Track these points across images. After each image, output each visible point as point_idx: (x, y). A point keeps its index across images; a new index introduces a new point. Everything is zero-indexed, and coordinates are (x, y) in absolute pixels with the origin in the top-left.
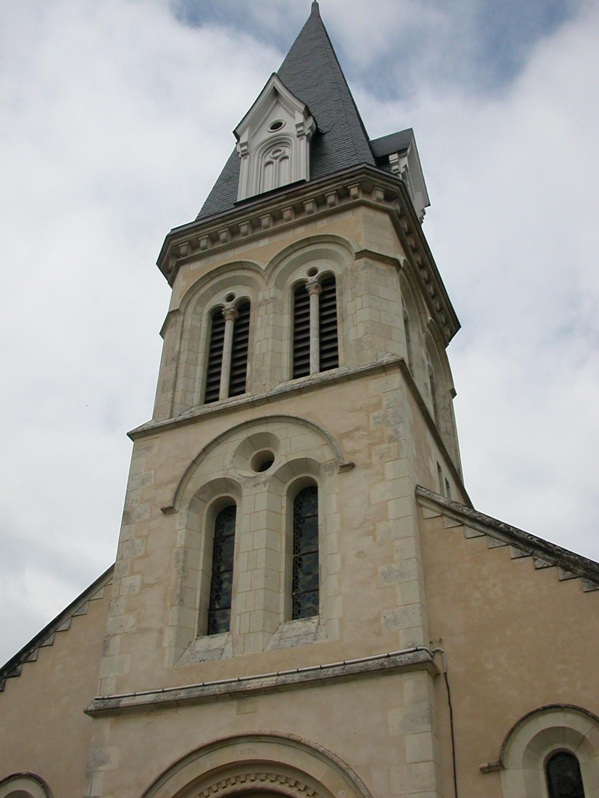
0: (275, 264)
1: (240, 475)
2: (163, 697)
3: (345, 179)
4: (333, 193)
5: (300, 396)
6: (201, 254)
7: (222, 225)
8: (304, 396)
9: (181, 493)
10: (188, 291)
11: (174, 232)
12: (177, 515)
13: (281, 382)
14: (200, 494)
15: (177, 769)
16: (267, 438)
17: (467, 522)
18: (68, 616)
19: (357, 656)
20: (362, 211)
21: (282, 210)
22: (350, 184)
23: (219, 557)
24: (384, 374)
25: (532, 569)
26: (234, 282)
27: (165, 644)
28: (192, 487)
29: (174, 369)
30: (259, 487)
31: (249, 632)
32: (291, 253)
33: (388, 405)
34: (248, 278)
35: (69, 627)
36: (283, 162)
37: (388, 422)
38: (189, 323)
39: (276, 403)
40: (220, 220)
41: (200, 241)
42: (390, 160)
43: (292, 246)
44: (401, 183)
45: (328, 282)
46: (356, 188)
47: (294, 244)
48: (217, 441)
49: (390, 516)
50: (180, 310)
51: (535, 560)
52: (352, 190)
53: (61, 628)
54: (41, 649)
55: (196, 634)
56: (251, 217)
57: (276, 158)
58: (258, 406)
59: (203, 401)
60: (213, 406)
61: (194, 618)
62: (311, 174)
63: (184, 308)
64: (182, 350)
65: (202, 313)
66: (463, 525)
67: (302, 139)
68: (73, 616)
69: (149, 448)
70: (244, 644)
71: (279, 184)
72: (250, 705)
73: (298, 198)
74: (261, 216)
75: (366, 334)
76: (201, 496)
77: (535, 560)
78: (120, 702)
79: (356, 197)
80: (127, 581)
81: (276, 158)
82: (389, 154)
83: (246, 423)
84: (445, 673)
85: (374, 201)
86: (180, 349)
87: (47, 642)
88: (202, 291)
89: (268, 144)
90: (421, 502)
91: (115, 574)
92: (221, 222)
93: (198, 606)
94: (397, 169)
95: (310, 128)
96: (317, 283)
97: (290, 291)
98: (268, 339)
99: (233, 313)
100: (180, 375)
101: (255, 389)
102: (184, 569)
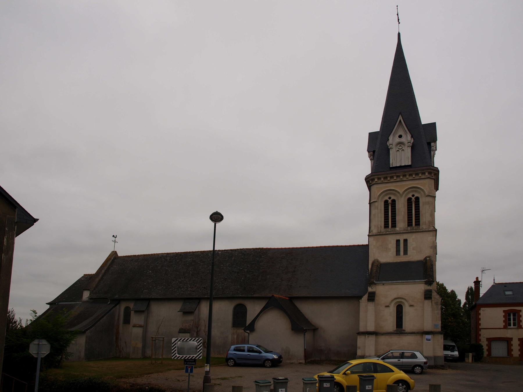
36: (403, 151)
45: (417, 199)
67: (409, 148)
94: (433, 149)
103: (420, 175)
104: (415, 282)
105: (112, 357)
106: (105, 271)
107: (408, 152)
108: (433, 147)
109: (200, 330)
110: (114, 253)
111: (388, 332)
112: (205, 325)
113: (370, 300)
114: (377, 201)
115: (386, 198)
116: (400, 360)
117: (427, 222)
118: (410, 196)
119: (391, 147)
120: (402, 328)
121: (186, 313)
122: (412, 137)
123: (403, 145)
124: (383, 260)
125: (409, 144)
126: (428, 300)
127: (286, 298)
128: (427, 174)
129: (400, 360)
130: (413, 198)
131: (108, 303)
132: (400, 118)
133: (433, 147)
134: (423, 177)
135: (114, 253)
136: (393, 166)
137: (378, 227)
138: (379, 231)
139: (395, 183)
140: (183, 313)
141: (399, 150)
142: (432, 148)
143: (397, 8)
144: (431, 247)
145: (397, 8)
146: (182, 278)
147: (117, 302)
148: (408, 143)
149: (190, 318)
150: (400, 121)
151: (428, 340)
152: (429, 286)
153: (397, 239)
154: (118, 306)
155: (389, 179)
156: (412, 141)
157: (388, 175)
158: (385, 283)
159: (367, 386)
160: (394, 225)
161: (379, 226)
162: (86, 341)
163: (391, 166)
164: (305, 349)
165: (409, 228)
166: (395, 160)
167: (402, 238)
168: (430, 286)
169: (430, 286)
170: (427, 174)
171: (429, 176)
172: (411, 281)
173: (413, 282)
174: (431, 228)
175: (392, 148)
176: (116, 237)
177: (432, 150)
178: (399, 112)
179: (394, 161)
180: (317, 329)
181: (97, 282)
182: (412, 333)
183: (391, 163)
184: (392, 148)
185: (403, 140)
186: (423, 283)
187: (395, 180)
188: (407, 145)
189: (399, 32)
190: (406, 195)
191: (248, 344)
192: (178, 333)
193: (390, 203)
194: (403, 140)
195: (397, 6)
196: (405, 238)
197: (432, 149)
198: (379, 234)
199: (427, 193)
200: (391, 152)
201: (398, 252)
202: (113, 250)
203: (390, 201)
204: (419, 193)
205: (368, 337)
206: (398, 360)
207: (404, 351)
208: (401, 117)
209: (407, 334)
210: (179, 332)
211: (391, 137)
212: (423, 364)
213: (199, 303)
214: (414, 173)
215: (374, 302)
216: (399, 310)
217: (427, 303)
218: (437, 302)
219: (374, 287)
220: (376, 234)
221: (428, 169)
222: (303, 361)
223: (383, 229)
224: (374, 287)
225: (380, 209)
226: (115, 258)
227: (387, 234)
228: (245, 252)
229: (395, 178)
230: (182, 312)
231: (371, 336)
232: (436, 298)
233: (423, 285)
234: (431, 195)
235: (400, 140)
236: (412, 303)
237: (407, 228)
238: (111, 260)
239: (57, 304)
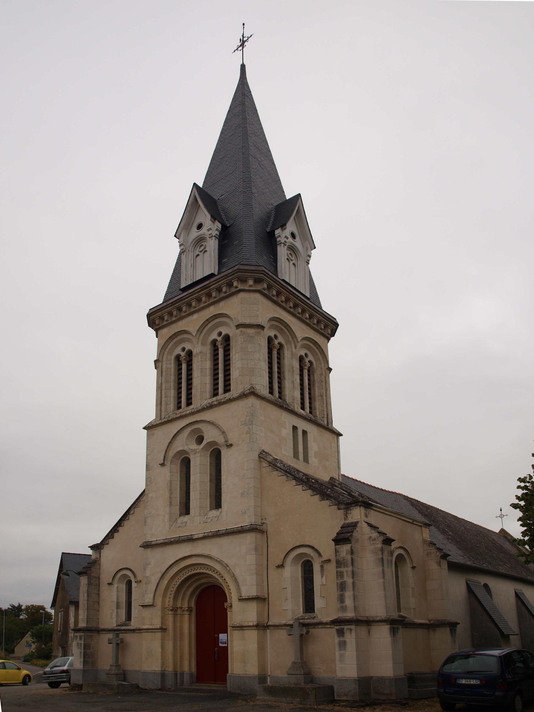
0: (200, 331)
1: (189, 448)
2: (166, 541)
3: (229, 276)
4: (224, 285)
6: (166, 324)
7: (172, 307)
8: (214, 409)
9: (166, 457)
10: (162, 348)
11: (151, 312)
12: (166, 467)
13: (206, 400)
14: (175, 457)
15: (172, 567)
16: (199, 430)
17: (278, 469)
18: (133, 508)
19: (231, 526)
20: (242, 295)
21: (201, 297)
23: (248, 418)
24: (246, 399)
25: (301, 490)
27: (166, 520)
28: (172, 453)
29: (160, 393)
30: (196, 454)
31: (195, 516)
32: (207, 324)
33: (247, 415)
35: (134, 512)
36: (206, 253)
37: (246, 424)
38: (165, 367)
39: (202, 413)
40: (171, 304)
41: (164, 316)
43: (207, 320)
44: (263, 272)
46: (236, 281)
47: (209, 318)
48: (179, 432)
49: (245, 469)
50: (159, 359)
51: (303, 486)
52: (234, 283)
53: (131, 513)
54: (125, 521)
55: (179, 515)
56: (186, 301)
57: (201, 252)
58: (195, 414)
59: (176, 408)
60: (179, 412)
61: (177, 509)
62: (221, 264)
63: (161, 358)
64: (163, 382)
65: (171, 359)
66: (277, 470)
67: (212, 239)
68: (134, 508)
69: (153, 434)
70: (193, 521)
71: (196, 279)
72: (196, 544)
73: (208, 289)
75: (240, 376)
76: (175, 458)
77: (303, 486)
78: (151, 543)
79: (236, 287)
80: (150, 495)
81: (201, 252)
83: (189, 423)
84: (266, 532)
85: (248, 287)
86: (162, 381)
87: (127, 518)
88: (169, 347)
89: (196, 241)
90: (261, 459)
91: (146, 492)
92: (171, 306)
93: (178, 504)
95: (217, 230)
96: (221, 342)
98: (199, 377)
99: (185, 359)
100: (163, 396)
101: (197, 403)
102: (170, 490)
123: (205, 243)
125: (210, 232)
141: (199, 253)
156: (218, 225)
195: (244, 24)
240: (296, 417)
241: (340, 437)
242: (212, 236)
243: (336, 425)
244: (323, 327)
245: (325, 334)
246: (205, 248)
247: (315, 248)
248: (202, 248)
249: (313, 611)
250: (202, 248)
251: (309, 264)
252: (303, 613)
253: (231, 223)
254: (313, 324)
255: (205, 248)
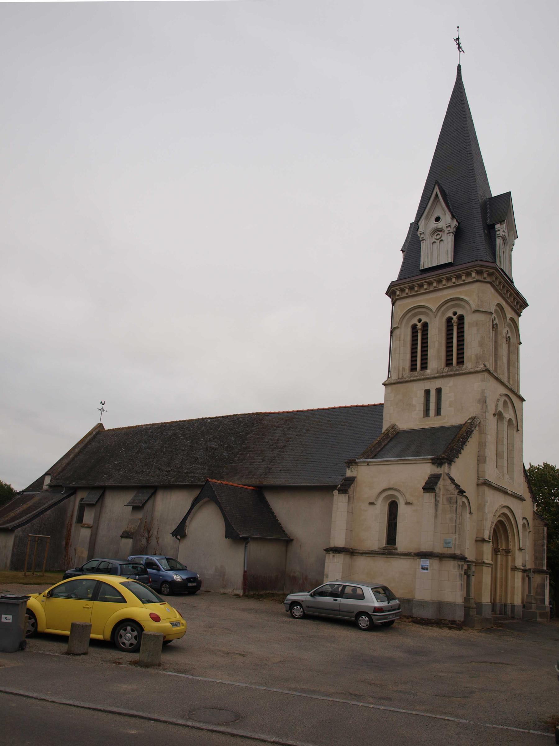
5: (423, 403)
21: (461, 275)
22: (420, 280)
26: (421, 313)
34: (425, 312)
36: (442, 242)
42: (496, 228)
45: (461, 318)
67: (450, 235)
74: (452, 276)
82: (458, 64)
94: (499, 234)
97: (409, 354)
103: (463, 278)
104: (415, 460)
105: (58, 571)
106: (81, 449)
107: (449, 240)
108: (499, 230)
109: (152, 534)
110: (100, 426)
111: (370, 549)
112: (158, 528)
113: (342, 490)
114: (399, 327)
115: (415, 321)
116: (336, 600)
117: (473, 356)
118: (450, 314)
119: (423, 238)
120: (395, 544)
121: (137, 508)
122: (453, 217)
123: (442, 233)
124: (403, 426)
125: (449, 229)
126: (429, 492)
127: (244, 486)
128: (474, 275)
129: (336, 600)
130: (455, 318)
131: (62, 493)
132: (437, 190)
133: (499, 230)
134: (469, 280)
135: (100, 424)
136: (426, 267)
137: (399, 370)
138: (400, 377)
139: (428, 295)
140: (133, 508)
141: (436, 241)
142: (498, 233)
143: (458, 30)
144: (479, 401)
145: (458, 30)
146: (152, 458)
147: (73, 491)
148: (447, 227)
149: (139, 515)
150: (437, 194)
151: (424, 569)
152: (438, 467)
153: (427, 388)
154: (72, 498)
155: (416, 289)
156: (455, 223)
157: (414, 283)
158: (370, 462)
159: (3, 616)
160: (424, 366)
161: (401, 368)
162: (14, 542)
163: (422, 268)
164: (245, 572)
165: (446, 369)
166: (428, 257)
167: (432, 386)
168: (441, 467)
169: (441, 467)
170: (474, 275)
171: (488, 280)
172: (410, 458)
173: (412, 460)
174: (480, 366)
175: (424, 240)
176: (104, 404)
177: (497, 236)
178: (435, 182)
179: (426, 260)
180: (292, 540)
181: (65, 465)
182: (407, 555)
183: (422, 263)
184: (424, 240)
185: (442, 224)
186: (428, 461)
187: (426, 289)
188: (446, 231)
189: (459, 64)
190: (444, 313)
191: (146, 554)
192: (120, 538)
193: (420, 329)
194: (442, 224)
195: (458, 27)
196: (437, 387)
197: (498, 235)
198: (398, 381)
199: (474, 307)
200: (423, 245)
201: (427, 413)
202: (99, 423)
203: (419, 325)
204: (463, 307)
205: (334, 556)
206: (335, 600)
207: (347, 584)
208: (438, 189)
209: (373, 555)
210: (122, 537)
211: (423, 220)
212: (372, 611)
213: (154, 494)
214: (454, 275)
215: (347, 495)
216: (393, 508)
217: (429, 497)
218: (451, 498)
219: (354, 469)
220: (395, 381)
221: (473, 267)
222: (240, 592)
223: (407, 373)
224: (354, 469)
225: (404, 340)
226: (98, 433)
227: (411, 381)
228: (237, 419)
229: (425, 287)
230: (131, 506)
231: (337, 555)
232: (448, 490)
233: (430, 465)
234: (481, 310)
235: (437, 225)
236: (410, 499)
237: (444, 368)
238: (92, 436)
239: (21, 494)
240: (518, 399)
241: (524, 402)
242: (451, 232)
243: (522, 393)
244: (498, 284)
245: (498, 289)
246: (441, 237)
247: (517, 238)
248: (438, 237)
249: (394, 543)
250: (438, 237)
251: (512, 251)
252: (386, 545)
253: (461, 220)
254: (496, 285)
255: (441, 237)
